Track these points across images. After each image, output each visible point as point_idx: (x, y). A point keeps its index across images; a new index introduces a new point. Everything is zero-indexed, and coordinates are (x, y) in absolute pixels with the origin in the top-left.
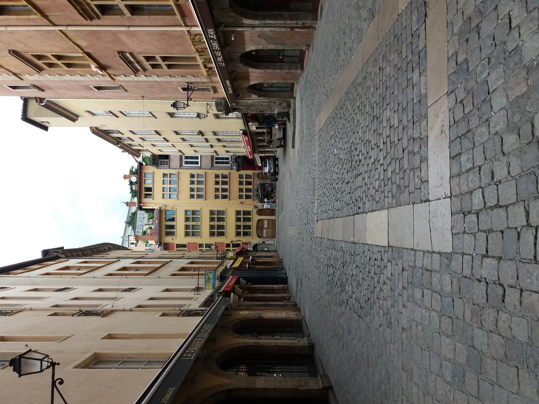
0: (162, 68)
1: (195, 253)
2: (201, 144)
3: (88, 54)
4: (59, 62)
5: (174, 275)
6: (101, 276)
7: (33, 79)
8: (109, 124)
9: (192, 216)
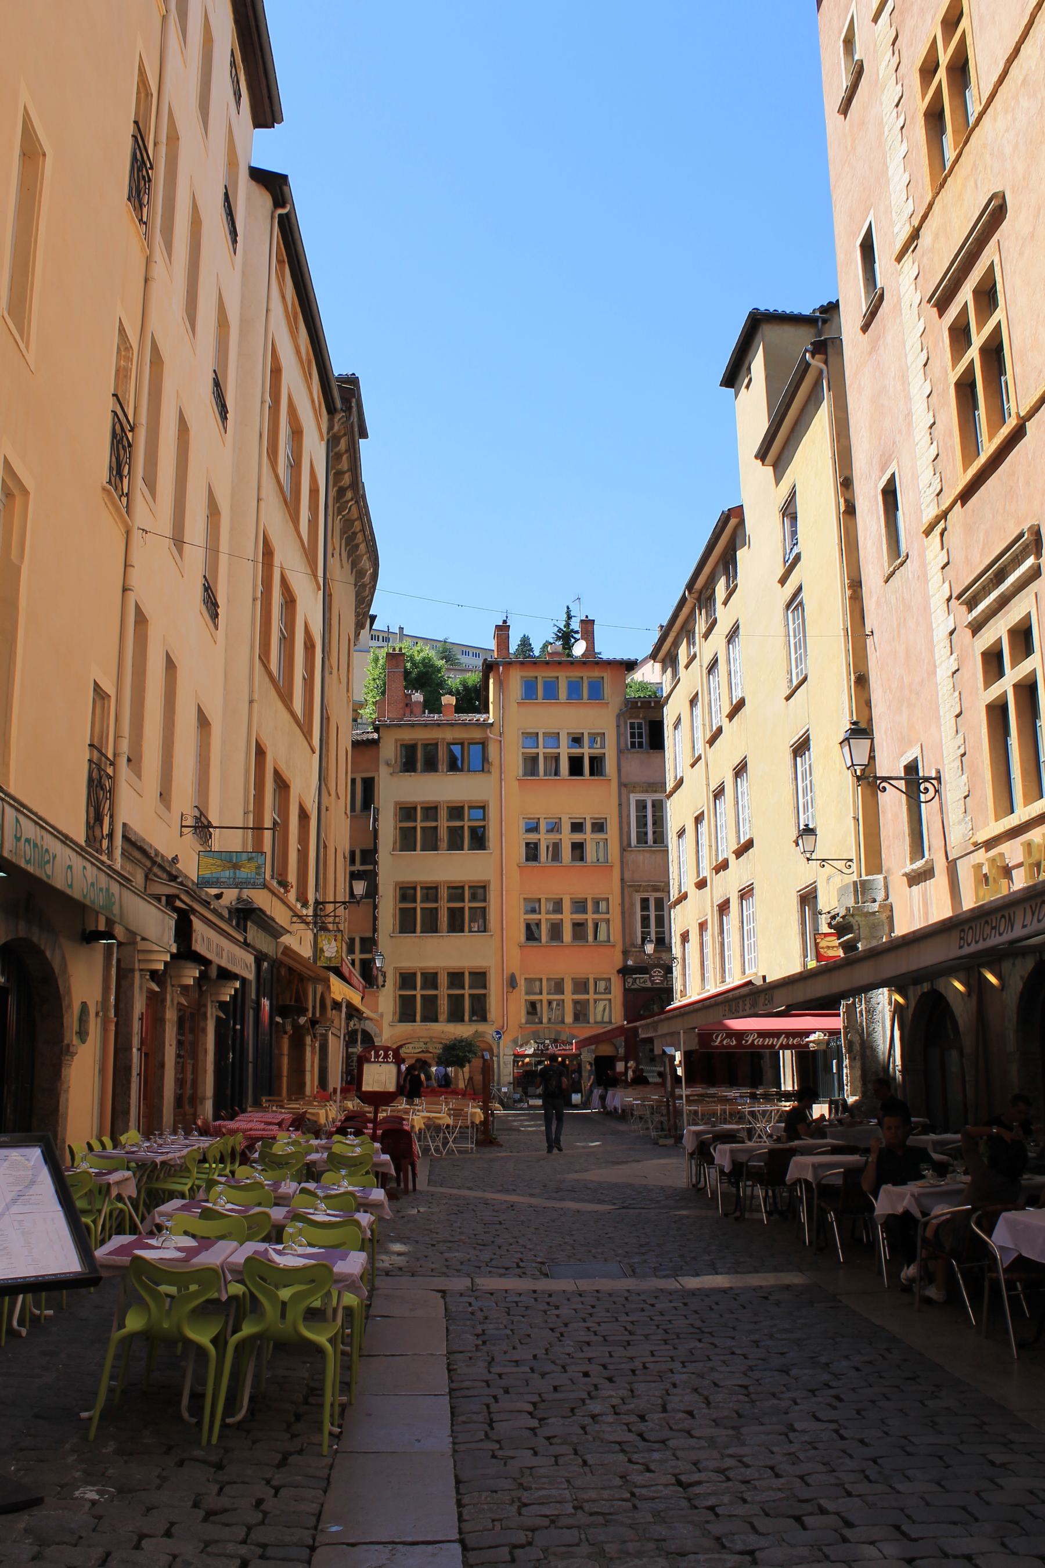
0: (988, 684)
1: (340, 834)
3: (1018, 434)
4: (973, 353)
5: (260, 752)
7: (902, 290)
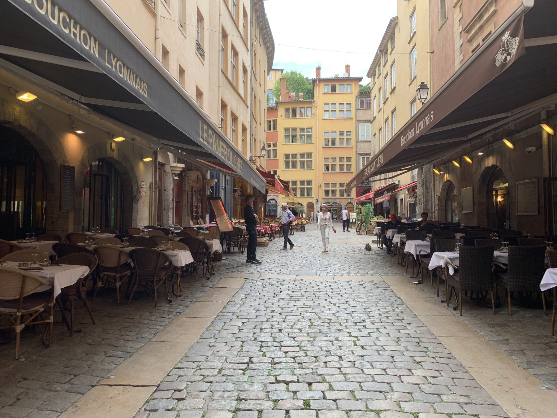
2: (383, 140)
6: (221, 20)
8: (401, 37)
9: (307, 134)
